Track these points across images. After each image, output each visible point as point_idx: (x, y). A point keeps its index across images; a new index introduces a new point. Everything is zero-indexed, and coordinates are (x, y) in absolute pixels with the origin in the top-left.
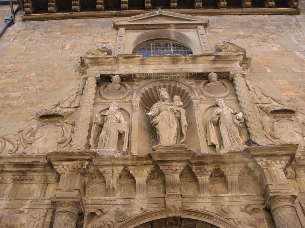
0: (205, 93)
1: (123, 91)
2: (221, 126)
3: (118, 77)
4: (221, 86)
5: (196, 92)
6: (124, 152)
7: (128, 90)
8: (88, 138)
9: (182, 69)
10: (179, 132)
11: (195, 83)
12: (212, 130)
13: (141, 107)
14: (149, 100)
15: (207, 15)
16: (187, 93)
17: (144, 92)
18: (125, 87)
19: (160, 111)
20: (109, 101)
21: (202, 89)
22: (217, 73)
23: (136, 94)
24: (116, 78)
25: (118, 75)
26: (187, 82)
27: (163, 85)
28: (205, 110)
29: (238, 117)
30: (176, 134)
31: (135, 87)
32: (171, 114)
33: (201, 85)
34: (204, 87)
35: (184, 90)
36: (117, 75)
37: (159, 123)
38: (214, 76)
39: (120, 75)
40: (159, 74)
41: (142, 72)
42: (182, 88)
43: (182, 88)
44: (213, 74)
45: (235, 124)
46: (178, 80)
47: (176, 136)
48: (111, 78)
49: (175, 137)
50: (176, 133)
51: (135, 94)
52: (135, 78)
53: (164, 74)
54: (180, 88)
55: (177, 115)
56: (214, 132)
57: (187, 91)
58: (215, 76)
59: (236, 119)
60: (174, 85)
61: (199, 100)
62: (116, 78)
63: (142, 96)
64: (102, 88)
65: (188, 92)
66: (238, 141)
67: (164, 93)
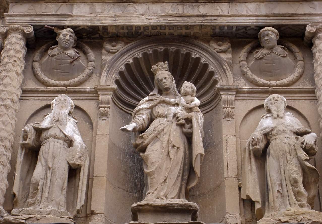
0: (250, 73)
1: (81, 65)
2: (271, 162)
3: (70, 34)
4: (283, 60)
5: (229, 73)
6: (78, 210)
7: (90, 63)
8: (11, 177)
9: (204, 16)
10: (186, 167)
11: (230, 49)
12: (251, 169)
13: (117, 102)
14: (136, 83)
15: (226, 91)
16: (212, 74)
17: (123, 67)
18: (85, 53)
19: (154, 117)
20: (52, 89)
21: (244, 65)
22: (278, 27)
23: (106, 74)
24: (66, 35)
25: (71, 30)
26: (212, 47)
27: (164, 50)
28: (244, 115)
29: (305, 144)
30: (181, 172)
31: (105, 55)
32: (174, 127)
33: (243, 54)
34: (247, 58)
35: (206, 66)
36: (69, 29)
37: (149, 148)
38: (271, 35)
39: (73, 27)
40: (155, 28)
41: (120, 22)
42: (203, 61)
43: (203, 61)
44: (270, 32)
45: (297, 158)
46: (167, 194)
47: (181, 175)
48: (56, 35)
49: (178, 176)
50: (180, 170)
51: (104, 74)
52: (105, 33)
53: (167, 28)
54: (198, 59)
55: (185, 128)
56: (254, 173)
57: (211, 68)
58: (273, 36)
59: (302, 147)
60: (187, 51)
61: (235, 93)
62: (66, 35)
63: (118, 77)
64: (37, 56)
65: (214, 69)
66: (299, 198)
67: (163, 73)
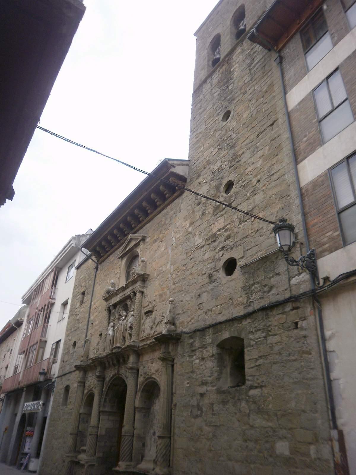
39: (112, 305)
